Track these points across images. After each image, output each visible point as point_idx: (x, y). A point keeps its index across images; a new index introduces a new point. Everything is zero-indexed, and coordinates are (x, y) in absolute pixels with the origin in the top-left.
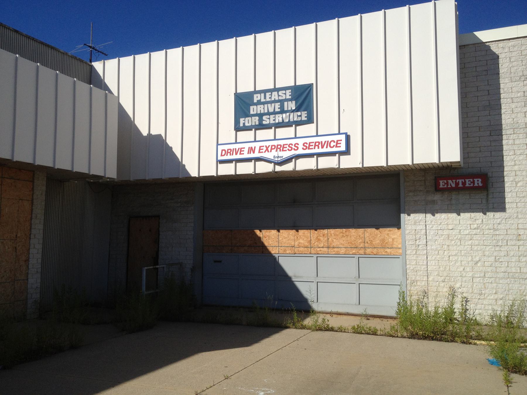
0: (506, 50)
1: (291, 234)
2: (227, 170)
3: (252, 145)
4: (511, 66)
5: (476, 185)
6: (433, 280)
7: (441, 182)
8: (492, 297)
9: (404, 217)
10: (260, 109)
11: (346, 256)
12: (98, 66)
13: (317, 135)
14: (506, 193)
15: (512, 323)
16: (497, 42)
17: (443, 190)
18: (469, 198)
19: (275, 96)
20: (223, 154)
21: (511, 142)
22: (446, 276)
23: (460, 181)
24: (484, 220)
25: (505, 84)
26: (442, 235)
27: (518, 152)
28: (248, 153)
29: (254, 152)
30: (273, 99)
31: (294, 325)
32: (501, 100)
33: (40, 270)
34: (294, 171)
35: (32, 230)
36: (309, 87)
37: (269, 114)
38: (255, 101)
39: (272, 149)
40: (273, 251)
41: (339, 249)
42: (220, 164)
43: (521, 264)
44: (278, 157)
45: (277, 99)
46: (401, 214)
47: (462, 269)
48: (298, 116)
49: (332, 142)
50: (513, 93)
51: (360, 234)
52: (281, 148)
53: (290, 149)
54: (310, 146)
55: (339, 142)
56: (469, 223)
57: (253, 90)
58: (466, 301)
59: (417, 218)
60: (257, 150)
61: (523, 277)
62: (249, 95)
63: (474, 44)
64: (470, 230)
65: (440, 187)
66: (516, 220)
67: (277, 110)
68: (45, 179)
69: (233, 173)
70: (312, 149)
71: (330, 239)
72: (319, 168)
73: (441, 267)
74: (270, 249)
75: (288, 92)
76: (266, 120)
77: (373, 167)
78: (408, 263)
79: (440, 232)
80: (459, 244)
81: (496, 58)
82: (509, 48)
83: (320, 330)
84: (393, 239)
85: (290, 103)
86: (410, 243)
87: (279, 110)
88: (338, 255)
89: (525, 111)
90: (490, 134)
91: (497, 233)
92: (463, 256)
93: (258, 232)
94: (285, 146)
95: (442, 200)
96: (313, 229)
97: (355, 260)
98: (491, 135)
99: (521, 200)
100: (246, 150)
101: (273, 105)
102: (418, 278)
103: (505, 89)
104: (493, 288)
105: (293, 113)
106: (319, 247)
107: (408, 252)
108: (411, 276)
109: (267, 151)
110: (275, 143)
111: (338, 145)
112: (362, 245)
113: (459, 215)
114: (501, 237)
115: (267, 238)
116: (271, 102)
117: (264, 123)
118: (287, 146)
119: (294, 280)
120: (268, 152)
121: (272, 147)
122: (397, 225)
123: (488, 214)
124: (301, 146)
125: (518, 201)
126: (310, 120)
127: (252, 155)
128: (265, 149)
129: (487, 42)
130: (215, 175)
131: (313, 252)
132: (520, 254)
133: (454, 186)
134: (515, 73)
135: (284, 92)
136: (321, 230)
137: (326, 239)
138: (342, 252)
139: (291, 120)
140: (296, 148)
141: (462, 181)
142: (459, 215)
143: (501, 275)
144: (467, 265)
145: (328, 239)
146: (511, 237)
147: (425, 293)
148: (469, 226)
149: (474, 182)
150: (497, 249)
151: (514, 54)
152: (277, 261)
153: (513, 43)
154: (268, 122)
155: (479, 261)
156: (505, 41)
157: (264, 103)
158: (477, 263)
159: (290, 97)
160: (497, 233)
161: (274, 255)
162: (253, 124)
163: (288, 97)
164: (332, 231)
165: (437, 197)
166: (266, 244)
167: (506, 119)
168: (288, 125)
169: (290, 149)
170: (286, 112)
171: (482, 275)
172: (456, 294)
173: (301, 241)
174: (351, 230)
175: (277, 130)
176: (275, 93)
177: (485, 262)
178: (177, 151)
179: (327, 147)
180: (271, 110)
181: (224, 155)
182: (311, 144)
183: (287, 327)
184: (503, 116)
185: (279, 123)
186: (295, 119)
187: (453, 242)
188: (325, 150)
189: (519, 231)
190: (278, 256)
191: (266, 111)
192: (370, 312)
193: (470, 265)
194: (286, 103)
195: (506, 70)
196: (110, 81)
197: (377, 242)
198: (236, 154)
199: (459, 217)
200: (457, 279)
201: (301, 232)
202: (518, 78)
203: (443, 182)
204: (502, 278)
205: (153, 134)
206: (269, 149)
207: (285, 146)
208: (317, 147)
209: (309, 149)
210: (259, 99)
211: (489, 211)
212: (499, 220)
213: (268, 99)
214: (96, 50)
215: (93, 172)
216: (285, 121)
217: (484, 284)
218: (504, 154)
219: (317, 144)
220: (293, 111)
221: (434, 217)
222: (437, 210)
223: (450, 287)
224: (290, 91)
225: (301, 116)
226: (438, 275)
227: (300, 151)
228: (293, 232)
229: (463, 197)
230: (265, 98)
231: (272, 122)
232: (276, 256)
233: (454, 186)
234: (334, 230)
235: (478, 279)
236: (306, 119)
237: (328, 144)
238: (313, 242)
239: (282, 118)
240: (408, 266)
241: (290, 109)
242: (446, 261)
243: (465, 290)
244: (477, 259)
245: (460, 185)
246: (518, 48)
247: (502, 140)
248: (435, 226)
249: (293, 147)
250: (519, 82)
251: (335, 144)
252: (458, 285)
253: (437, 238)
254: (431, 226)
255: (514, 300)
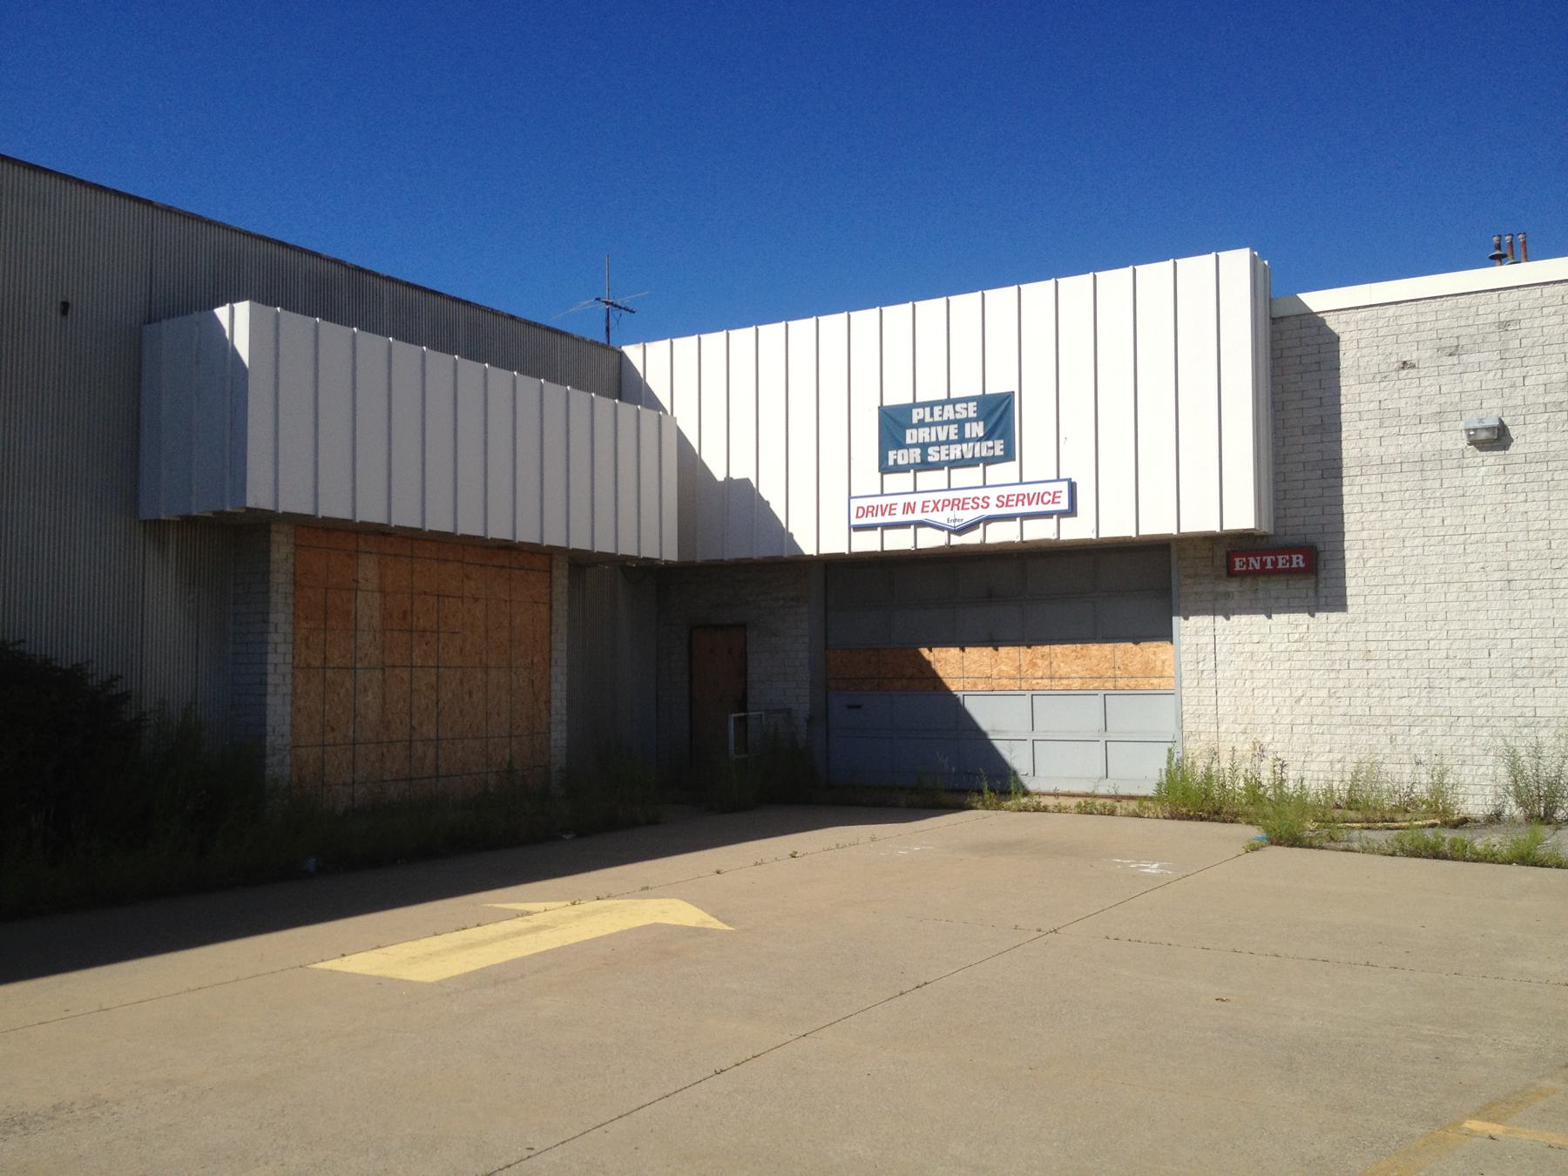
0: (1352, 327)
1: (985, 654)
2: (866, 543)
3: (911, 499)
4: (1358, 355)
5: (1294, 565)
6: (1227, 731)
7: (1237, 560)
8: (1324, 759)
9: (1177, 621)
10: (923, 435)
11: (1084, 692)
12: (633, 352)
13: (1021, 483)
14: (1347, 579)
15: (1357, 801)
16: (1337, 313)
17: (1243, 575)
18: (1285, 587)
19: (949, 413)
20: (860, 514)
21: (1356, 489)
22: (1249, 724)
23: (1269, 559)
24: (1311, 626)
25: (1349, 387)
26: (1242, 653)
27: (1368, 508)
28: (903, 513)
29: (913, 512)
30: (945, 418)
31: (983, 805)
32: (1342, 415)
33: (565, 718)
34: (983, 544)
35: (553, 652)
36: (1008, 397)
37: (938, 443)
38: (915, 421)
39: (944, 506)
40: (954, 686)
41: (1070, 681)
42: (854, 531)
43: (1371, 701)
44: (955, 520)
45: (952, 417)
46: (1173, 618)
47: (1274, 711)
48: (988, 448)
49: (1046, 495)
50: (1362, 404)
51: (1107, 653)
52: (961, 505)
53: (975, 506)
54: (1008, 500)
55: (1057, 495)
56: (1286, 631)
57: (911, 401)
58: (1282, 766)
59: (1200, 624)
60: (919, 507)
61: (1374, 723)
62: (906, 410)
63: (1297, 316)
64: (1288, 644)
65: (1267, 567)
66: (1365, 625)
67: (953, 437)
68: (567, 566)
69: (879, 549)
70: (1012, 506)
71: (1054, 664)
72: (1025, 539)
73: (1240, 707)
74: (948, 682)
75: (972, 406)
76: (934, 455)
77: (1118, 537)
78: (1184, 703)
79: (1238, 648)
80: (1269, 667)
81: (1334, 340)
82: (1357, 323)
83: (1026, 811)
84: (1163, 662)
85: (974, 424)
86: (1189, 667)
87: (956, 437)
88: (1068, 692)
89: (1381, 435)
90: (1322, 475)
91: (1333, 648)
92: (1275, 688)
93: (925, 652)
94: (966, 501)
95: (1239, 592)
96: (1023, 645)
97: (1099, 699)
98: (1323, 478)
99: (1371, 591)
100: (900, 508)
101: (946, 427)
102: (1201, 728)
103: (1350, 397)
104: (1326, 743)
105: (979, 443)
106: (1035, 678)
107: (1185, 684)
108: (1189, 726)
109: (935, 510)
110: (951, 495)
111: (1056, 500)
112: (1110, 673)
113: (1270, 617)
114: (1337, 656)
115: (943, 662)
116: (942, 423)
117: (930, 459)
118: (970, 501)
119: (991, 737)
120: (938, 510)
121: (944, 503)
122: (1166, 635)
123: (1317, 615)
124: (993, 502)
125: (1367, 593)
126: (1008, 455)
127: (910, 517)
128: (932, 505)
129: (1319, 313)
130: (847, 553)
131: (1024, 686)
132: (1369, 684)
133: (1258, 567)
134: (1365, 368)
135: (964, 405)
136: (1039, 647)
137: (1047, 662)
138: (1075, 685)
139: (977, 455)
140: (985, 505)
141: (1272, 560)
142: (1270, 617)
143: (1339, 720)
144: (1282, 703)
145: (1051, 663)
146: (1355, 655)
147: (1214, 754)
148: (1286, 636)
149: (1291, 561)
150: (1333, 675)
151: (1365, 334)
152: (960, 704)
153: (1364, 313)
154: (936, 459)
155: (1303, 696)
156: (1350, 311)
157: (929, 425)
158: (1298, 700)
159: (975, 415)
160: (1333, 648)
161: (955, 693)
162: (912, 461)
163: (972, 415)
164: (1058, 649)
165: (1233, 586)
166: (941, 674)
167: (1350, 450)
168: (972, 462)
169: (975, 506)
170: (968, 441)
171: (1308, 720)
172: (1265, 754)
173: (1004, 668)
174: (1090, 645)
175: (953, 471)
176: (949, 408)
177: (1313, 699)
178: (778, 509)
179: (1037, 503)
180: (942, 437)
181: (861, 517)
182: (1011, 498)
183: (971, 808)
184: (1344, 444)
185: (955, 461)
186: (984, 454)
187: (1260, 664)
188: (1034, 508)
189: (1369, 644)
190: (964, 695)
191: (934, 439)
192: (1123, 791)
193: (1287, 704)
194: (967, 426)
195: (1351, 363)
196: (657, 382)
197: (1136, 666)
198: (883, 514)
199: (1270, 621)
200: (1266, 728)
201: (1003, 650)
202: (1370, 377)
203: (1240, 561)
204: (1340, 726)
205: (735, 478)
206: (940, 506)
207: (966, 501)
208: (1020, 503)
209: (1007, 506)
210: (921, 417)
211: (1319, 610)
212: (1335, 626)
213: (937, 418)
214: (616, 306)
215: (645, 553)
216: (966, 457)
217: (1311, 735)
218: (1345, 511)
219: (1021, 497)
220: (980, 440)
221: (1228, 622)
222: (1233, 610)
223: (1254, 743)
224: (975, 403)
225: (993, 448)
226: (1235, 722)
227: (993, 511)
228: (989, 651)
229: (1277, 587)
230: (932, 415)
231: (944, 458)
232: (960, 695)
233: (1258, 567)
234: (1061, 646)
235: (1301, 728)
236: (1002, 453)
237: (1040, 497)
238: (1024, 668)
239: (962, 450)
240: (1185, 708)
241: (974, 435)
242: (1247, 697)
243: (1279, 746)
244: (1299, 693)
245: (1269, 566)
246: (1372, 323)
247: (1342, 486)
248: (1229, 637)
249: (980, 502)
250: (1371, 385)
251: (1051, 498)
252: (1268, 738)
253: (1233, 658)
254: (1223, 637)
255: (1361, 762)
